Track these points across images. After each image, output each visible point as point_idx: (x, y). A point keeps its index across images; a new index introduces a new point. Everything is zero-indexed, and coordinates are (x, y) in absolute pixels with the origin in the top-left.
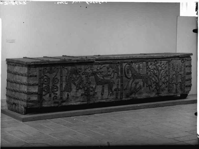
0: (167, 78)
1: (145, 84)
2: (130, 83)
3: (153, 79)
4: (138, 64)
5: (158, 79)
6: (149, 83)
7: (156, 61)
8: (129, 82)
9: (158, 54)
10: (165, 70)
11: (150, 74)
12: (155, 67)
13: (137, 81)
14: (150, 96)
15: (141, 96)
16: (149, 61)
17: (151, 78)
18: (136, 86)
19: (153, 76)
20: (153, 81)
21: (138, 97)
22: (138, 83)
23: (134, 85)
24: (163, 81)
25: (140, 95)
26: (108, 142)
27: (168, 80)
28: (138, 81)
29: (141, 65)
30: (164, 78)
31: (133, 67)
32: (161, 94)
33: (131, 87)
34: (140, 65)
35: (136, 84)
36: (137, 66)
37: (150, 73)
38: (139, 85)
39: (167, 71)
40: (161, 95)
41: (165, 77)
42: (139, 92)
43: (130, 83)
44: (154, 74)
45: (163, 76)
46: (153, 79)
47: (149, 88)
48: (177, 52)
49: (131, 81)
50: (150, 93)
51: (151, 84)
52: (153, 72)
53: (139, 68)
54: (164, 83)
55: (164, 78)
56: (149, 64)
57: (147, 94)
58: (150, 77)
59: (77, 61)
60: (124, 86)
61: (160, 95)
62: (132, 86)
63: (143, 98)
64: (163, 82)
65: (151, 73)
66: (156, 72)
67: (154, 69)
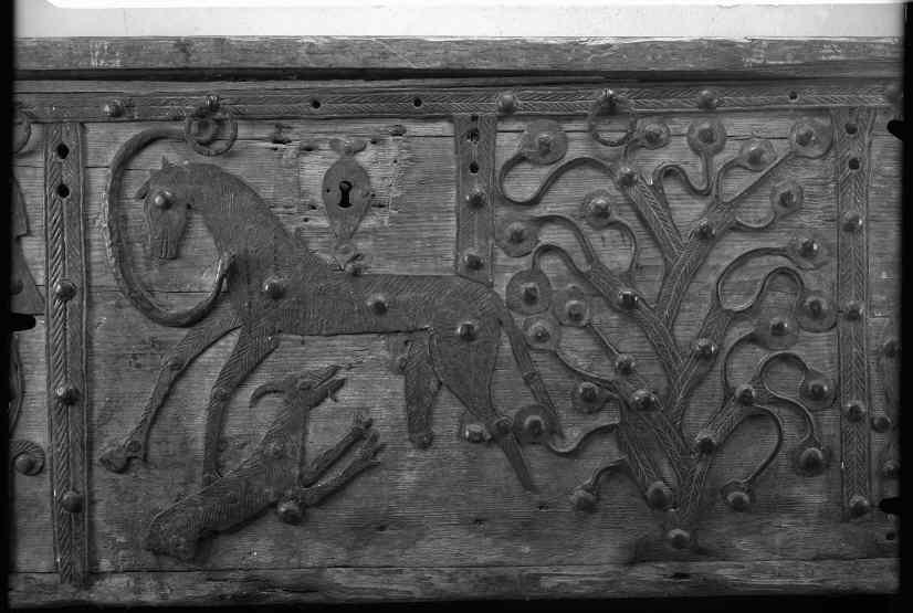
0: (817, 349)
1: (447, 414)
2: (201, 388)
3: (570, 357)
4: (334, 145)
5: (664, 352)
6: (512, 400)
7: (610, 110)
8: (181, 369)
9: (446, 37)
10: (775, 241)
11: (521, 276)
12: (601, 190)
13: (315, 357)
14: (537, 577)
15: (389, 570)
16: (508, 112)
17: (542, 337)
18: (295, 425)
19: (575, 317)
20: (572, 372)
21: (340, 578)
22: (331, 385)
23: (254, 419)
24: (742, 385)
25: (368, 556)
26: (20, 288)
27: (831, 373)
28: (324, 364)
29: (379, 164)
30: (752, 339)
31: (240, 185)
32: (722, 554)
33: (217, 442)
34: (364, 158)
35: (312, 394)
36: (314, 170)
37: (523, 263)
38: (335, 414)
39: (807, 251)
40: (727, 572)
41: (778, 330)
42: (343, 510)
43: (201, 388)
44: (592, 279)
45: (738, 317)
46: (577, 349)
47: (519, 467)
48: (193, 65)
49: (217, 357)
50: (525, 529)
51: (547, 407)
52: (580, 259)
53: (345, 193)
54: (754, 412)
55: (752, 339)
56: (508, 142)
57: (486, 552)
58: (520, 320)
59: (847, 53)
60: (106, 418)
61: (700, 567)
62: (233, 429)
63: (418, 593)
64: (745, 399)
65: (535, 273)
66: (617, 256)
67: (583, 225)
